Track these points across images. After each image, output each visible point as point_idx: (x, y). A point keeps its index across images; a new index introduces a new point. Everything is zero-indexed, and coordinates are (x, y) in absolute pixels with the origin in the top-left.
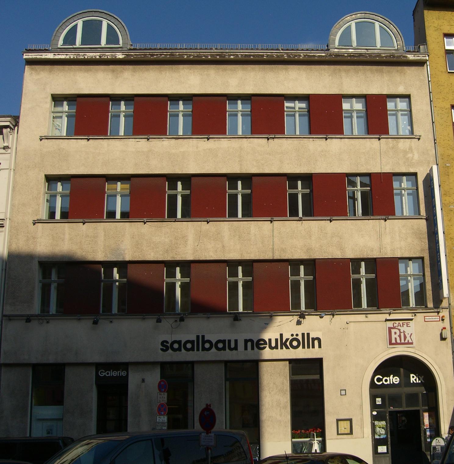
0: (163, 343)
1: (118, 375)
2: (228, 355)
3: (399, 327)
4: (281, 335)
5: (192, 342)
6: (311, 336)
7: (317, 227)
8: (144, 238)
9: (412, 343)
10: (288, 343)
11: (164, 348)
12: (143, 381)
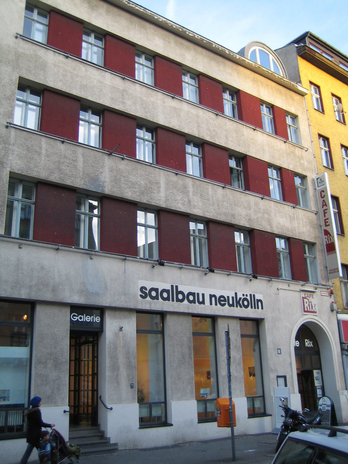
0: (142, 289)
1: (92, 321)
2: (197, 309)
3: (308, 298)
4: (236, 294)
5: (167, 291)
6: (256, 298)
7: (254, 201)
8: (122, 174)
9: (315, 312)
10: (241, 302)
11: (144, 295)
12: (121, 329)
